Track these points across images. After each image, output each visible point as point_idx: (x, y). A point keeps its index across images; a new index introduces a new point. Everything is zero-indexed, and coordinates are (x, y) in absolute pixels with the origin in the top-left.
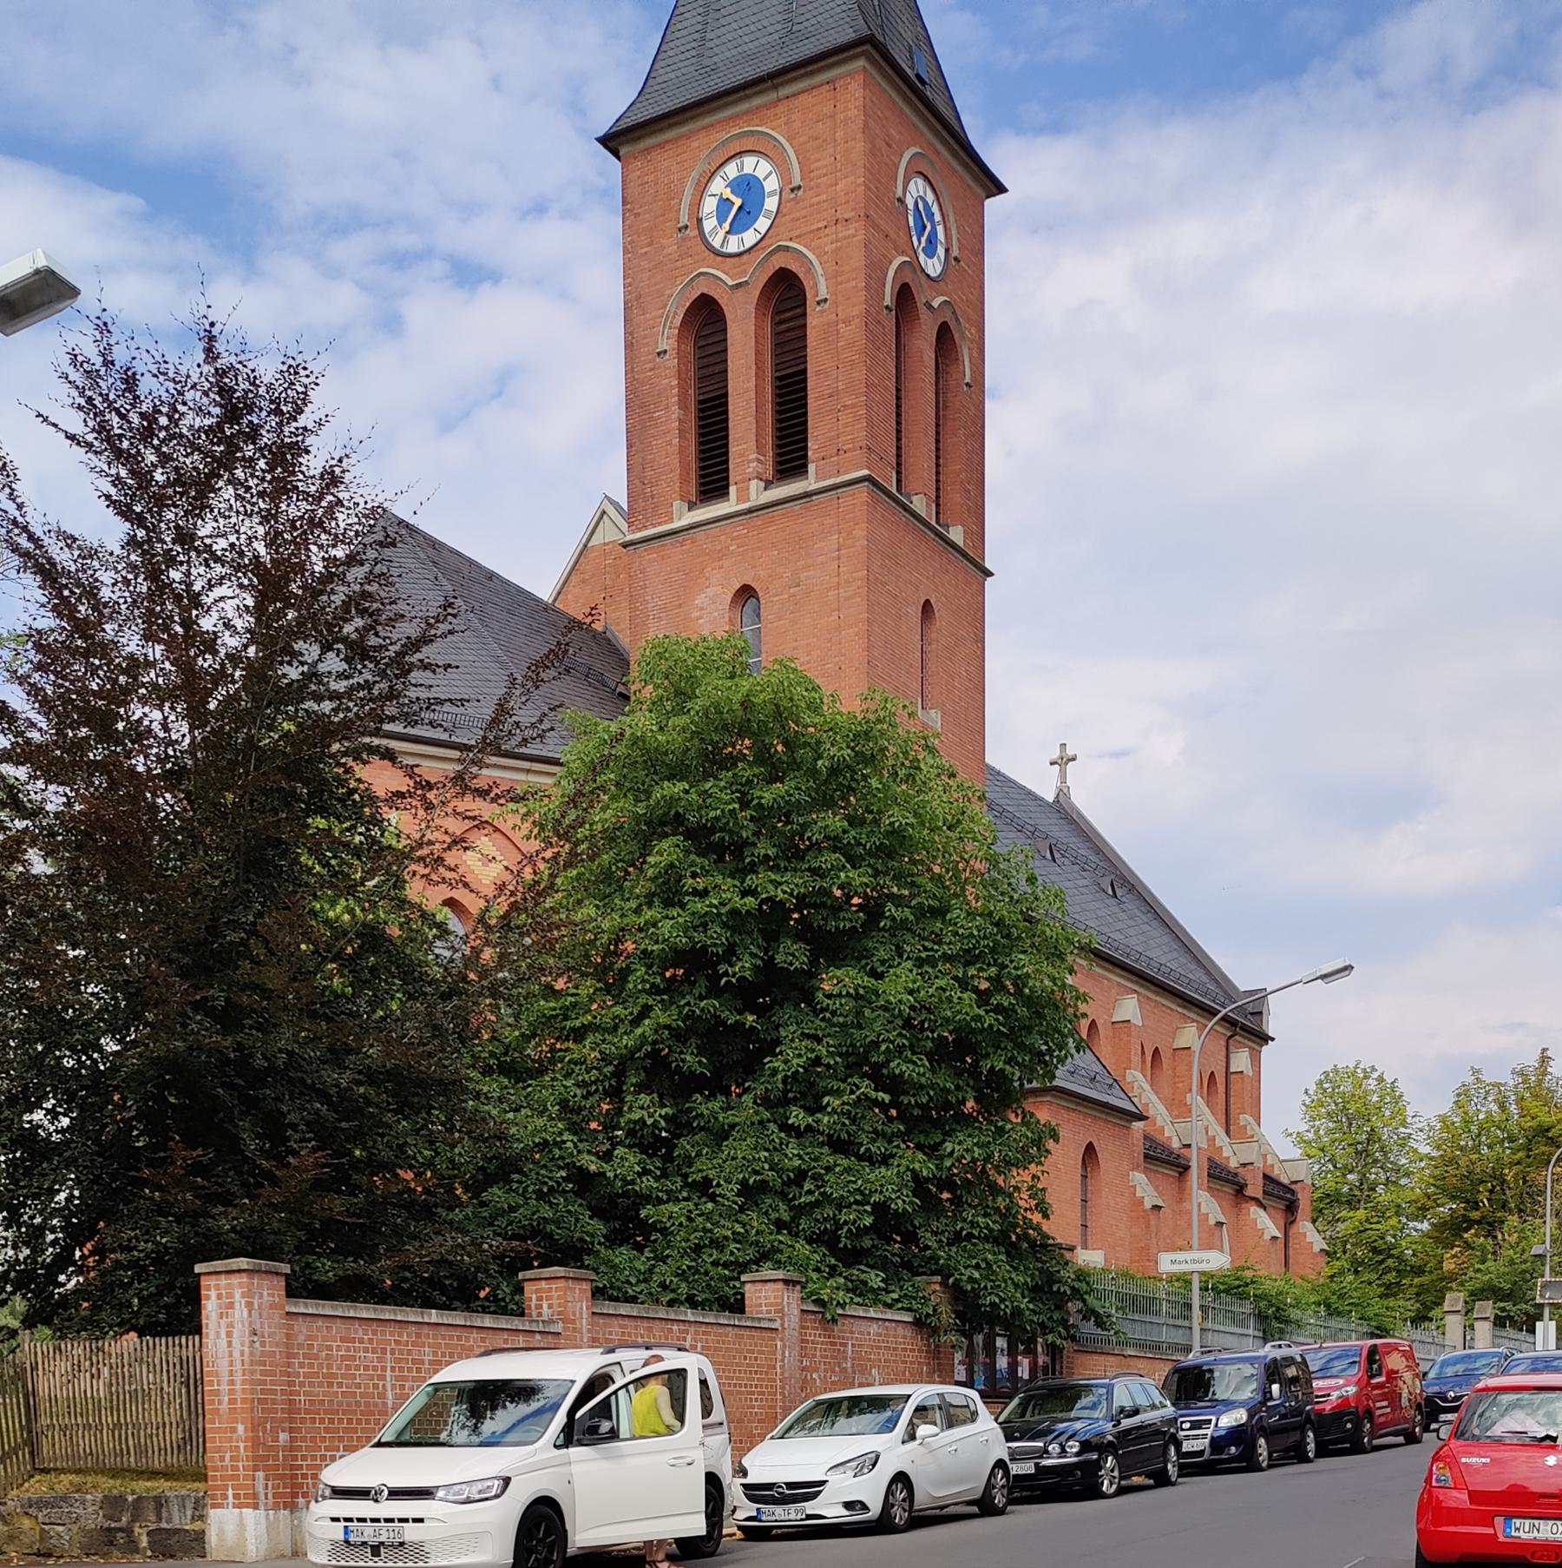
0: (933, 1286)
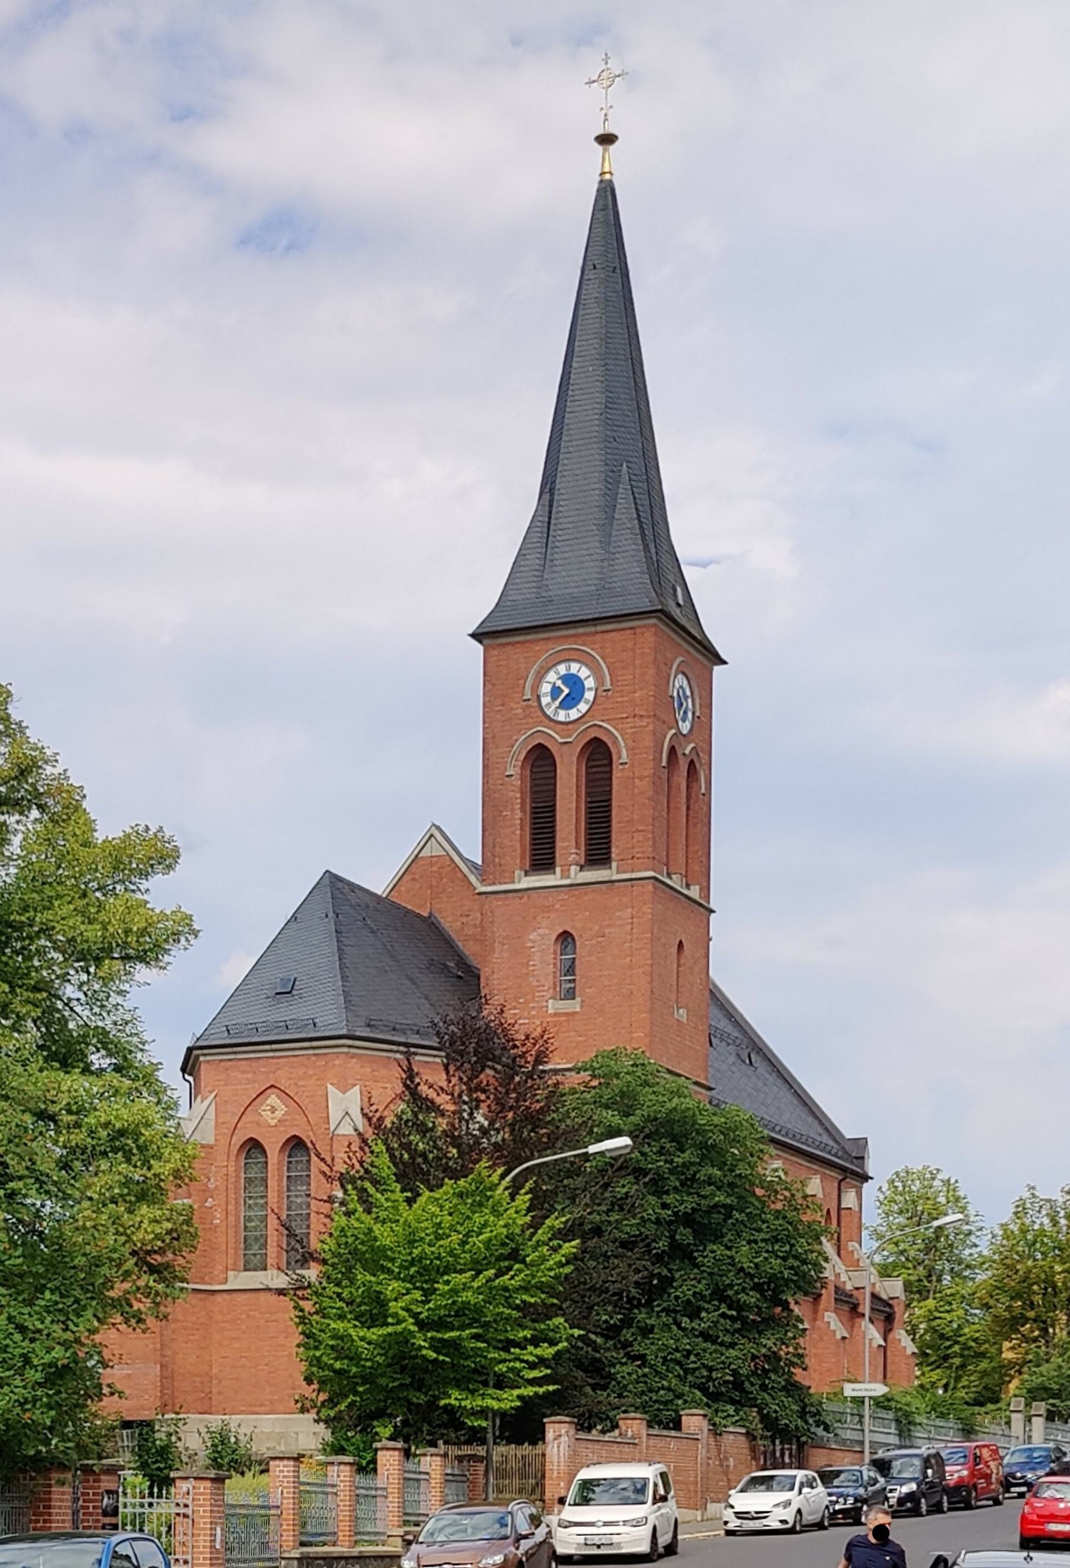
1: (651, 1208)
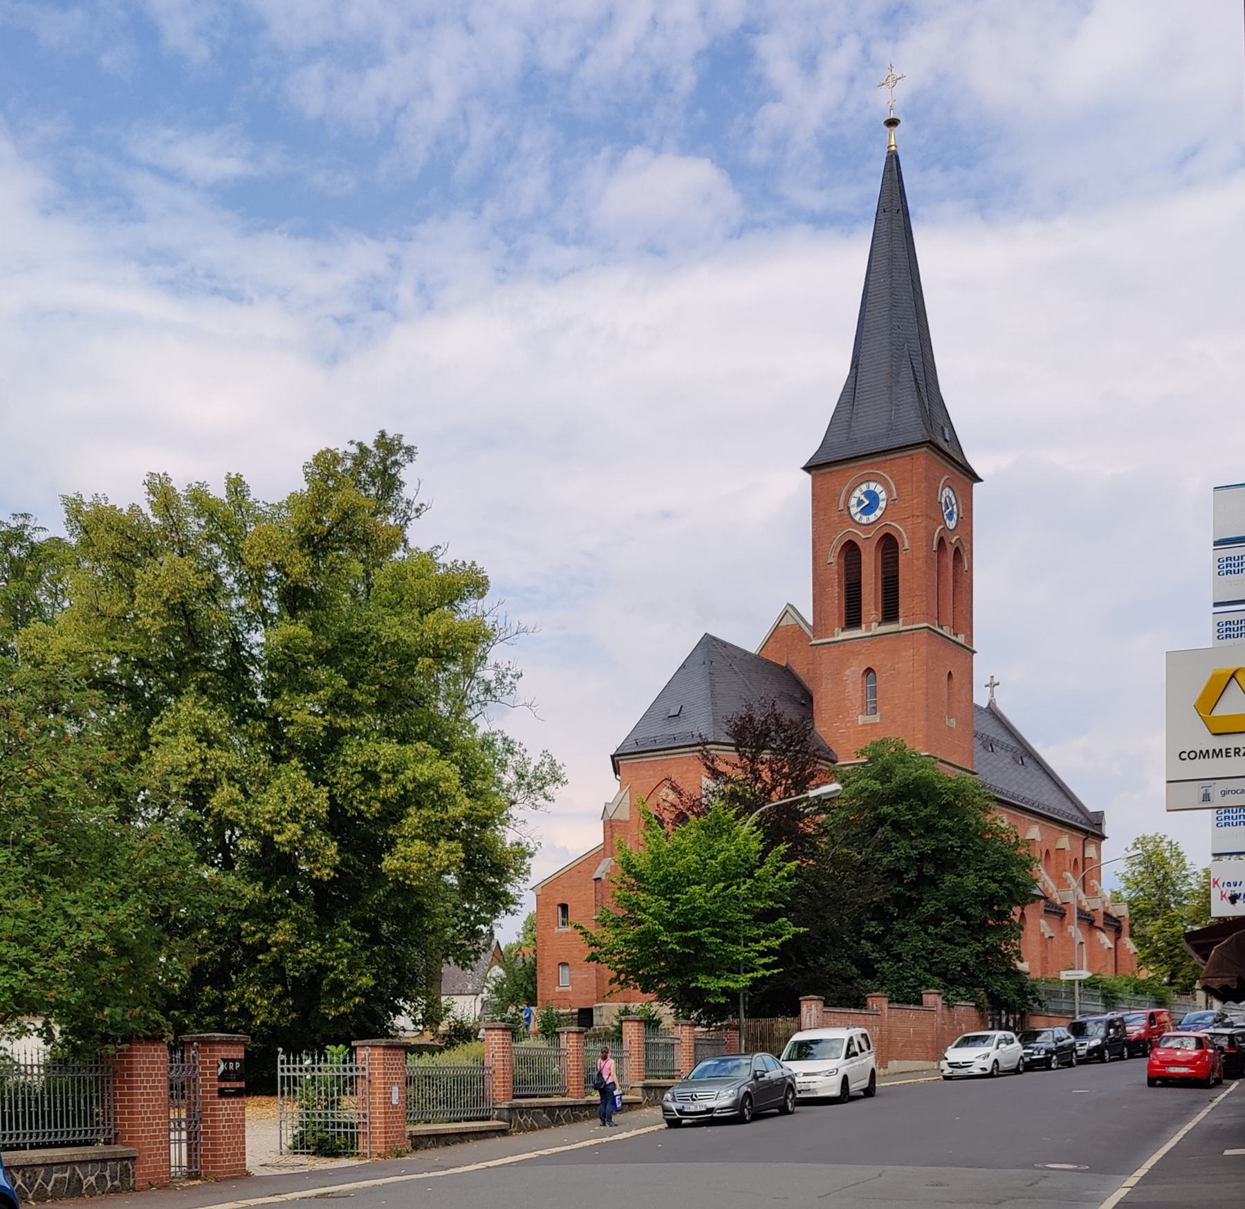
0: (981, 992)
1: (903, 848)
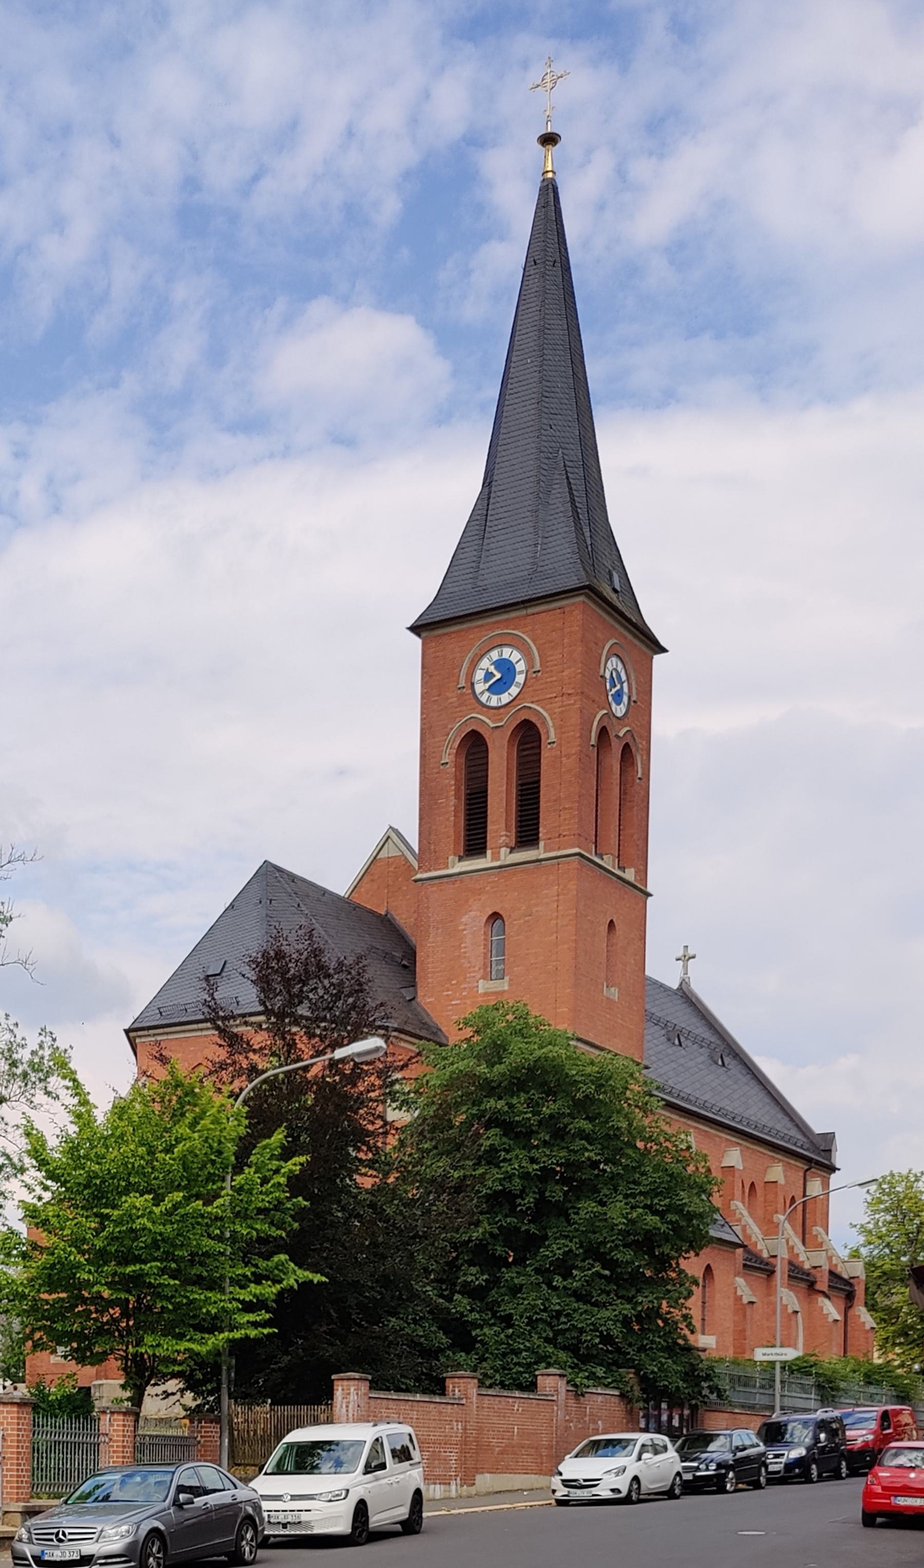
0: (630, 1375)
1: (518, 1161)
